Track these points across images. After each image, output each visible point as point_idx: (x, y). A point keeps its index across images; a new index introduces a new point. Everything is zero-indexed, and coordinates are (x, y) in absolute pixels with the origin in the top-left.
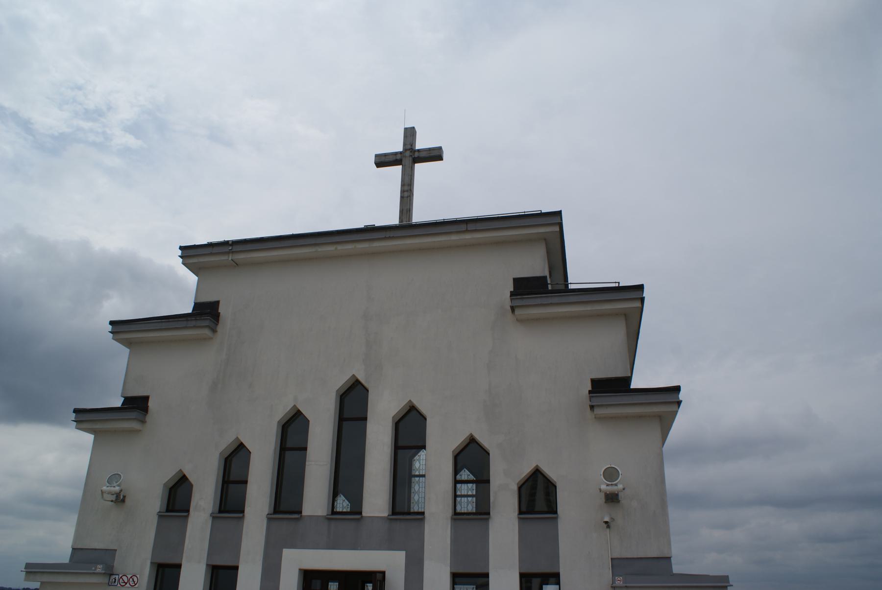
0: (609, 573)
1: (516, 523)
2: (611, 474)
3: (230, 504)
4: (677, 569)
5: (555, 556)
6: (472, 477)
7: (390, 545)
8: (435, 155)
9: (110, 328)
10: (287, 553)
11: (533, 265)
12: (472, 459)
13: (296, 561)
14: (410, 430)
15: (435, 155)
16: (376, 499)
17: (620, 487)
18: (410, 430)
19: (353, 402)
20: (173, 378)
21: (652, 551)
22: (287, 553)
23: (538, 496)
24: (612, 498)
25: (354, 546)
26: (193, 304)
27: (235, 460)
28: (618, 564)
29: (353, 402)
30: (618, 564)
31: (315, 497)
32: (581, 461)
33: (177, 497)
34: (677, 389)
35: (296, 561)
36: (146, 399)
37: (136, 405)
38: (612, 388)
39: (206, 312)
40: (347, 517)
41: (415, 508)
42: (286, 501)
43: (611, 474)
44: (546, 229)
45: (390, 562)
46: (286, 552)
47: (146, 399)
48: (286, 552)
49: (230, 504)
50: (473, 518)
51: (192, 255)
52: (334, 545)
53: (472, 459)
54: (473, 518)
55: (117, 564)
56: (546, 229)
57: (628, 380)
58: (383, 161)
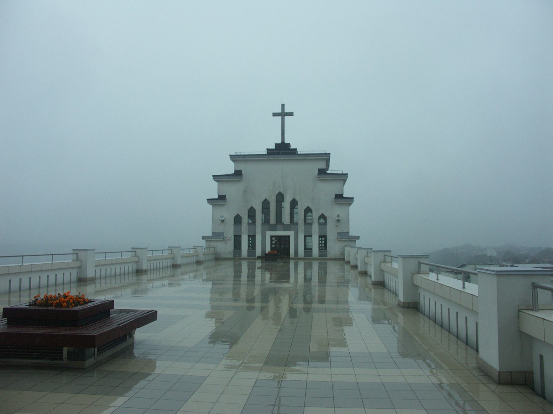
0: (336, 235)
2: (338, 216)
4: (350, 234)
5: (326, 233)
6: (467, 412)
8: (291, 114)
11: (322, 165)
14: (294, 204)
15: (291, 114)
16: (286, 219)
18: (294, 204)
19: (280, 197)
20: (233, 190)
21: (345, 231)
24: (338, 221)
27: (252, 213)
28: (338, 233)
29: (280, 197)
31: (273, 220)
32: (334, 213)
33: (238, 220)
34: (353, 198)
36: (225, 196)
37: (222, 198)
38: (339, 197)
39: (238, 173)
41: (295, 222)
42: (266, 221)
43: (338, 216)
44: (326, 157)
45: (291, 234)
47: (225, 196)
50: (308, 224)
51: (234, 158)
53: (308, 210)
56: (326, 157)
57: (342, 195)
58: (275, 115)
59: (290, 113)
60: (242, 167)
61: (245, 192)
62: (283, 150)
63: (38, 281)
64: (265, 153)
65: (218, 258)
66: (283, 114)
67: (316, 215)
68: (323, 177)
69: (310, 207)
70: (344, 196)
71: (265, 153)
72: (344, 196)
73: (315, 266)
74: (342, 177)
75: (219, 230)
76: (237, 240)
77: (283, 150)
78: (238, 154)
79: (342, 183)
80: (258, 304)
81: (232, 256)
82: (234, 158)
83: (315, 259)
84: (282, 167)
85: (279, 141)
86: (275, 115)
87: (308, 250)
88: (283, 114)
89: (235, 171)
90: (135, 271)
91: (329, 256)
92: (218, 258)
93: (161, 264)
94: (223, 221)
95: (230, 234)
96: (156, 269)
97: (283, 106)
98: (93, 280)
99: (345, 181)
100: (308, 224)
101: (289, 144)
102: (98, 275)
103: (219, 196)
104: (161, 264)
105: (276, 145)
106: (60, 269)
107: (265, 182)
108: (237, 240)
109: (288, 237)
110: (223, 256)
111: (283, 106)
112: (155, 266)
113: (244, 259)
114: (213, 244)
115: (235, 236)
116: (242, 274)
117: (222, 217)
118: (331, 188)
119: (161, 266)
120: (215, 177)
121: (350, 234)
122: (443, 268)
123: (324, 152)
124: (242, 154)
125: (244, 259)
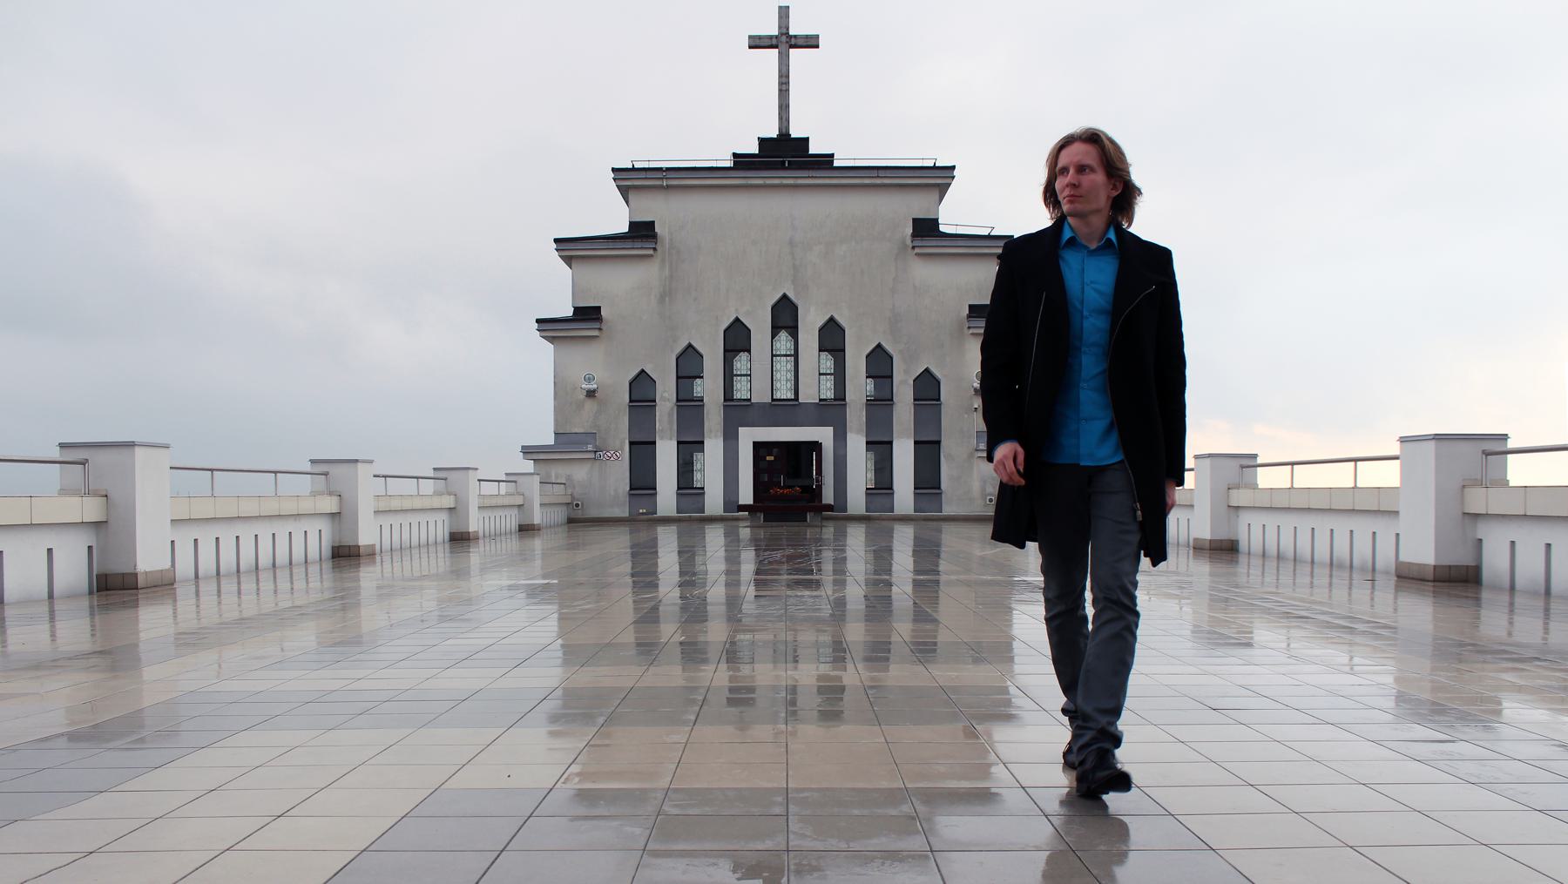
8: (811, 42)
11: (917, 205)
13: (748, 436)
15: (811, 42)
19: (785, 316)
20: (618, 286)
29: (785, 316)
33: (641, 390)
37: (587, 315)
39: (642, 231)
45: (823, 435)
51: (630, 180)
58: (757, 43)
59: (780, 17)
61: (666, 295)
62: (783, 156)
65: (578, 520)
66: (784, 42)
67: (810, 324)
68: (931, 245)
71: (729, 164)
73: (903, 542)
77: (783, 156)
80: (902, 629)
81: (624, 512)
83: (904, 519)
85: (773, 133)
86: (757, 43)
87: (882, 484)
88: (784, 42)
89: (631, 224)
90: (327, 552)
91: (948, 509)
92: (578, 520)
94: (591, 394)
96: (402, 550)
97: (784, 13)
98: (164, 585)
99: (943, 189)
100: (881, 403)
101: (805, 141)
102: (184, 568)
103: (577, 310)
110: (594, 513)
111: (784, 13)
113: (666, 521)
114: (559, 472)
116: (627, 567)
117: (589, 379)
119: (415, 542)
122: (686, 469)
123: (985, 232)
124: (653, 165)
125: (666, 521)
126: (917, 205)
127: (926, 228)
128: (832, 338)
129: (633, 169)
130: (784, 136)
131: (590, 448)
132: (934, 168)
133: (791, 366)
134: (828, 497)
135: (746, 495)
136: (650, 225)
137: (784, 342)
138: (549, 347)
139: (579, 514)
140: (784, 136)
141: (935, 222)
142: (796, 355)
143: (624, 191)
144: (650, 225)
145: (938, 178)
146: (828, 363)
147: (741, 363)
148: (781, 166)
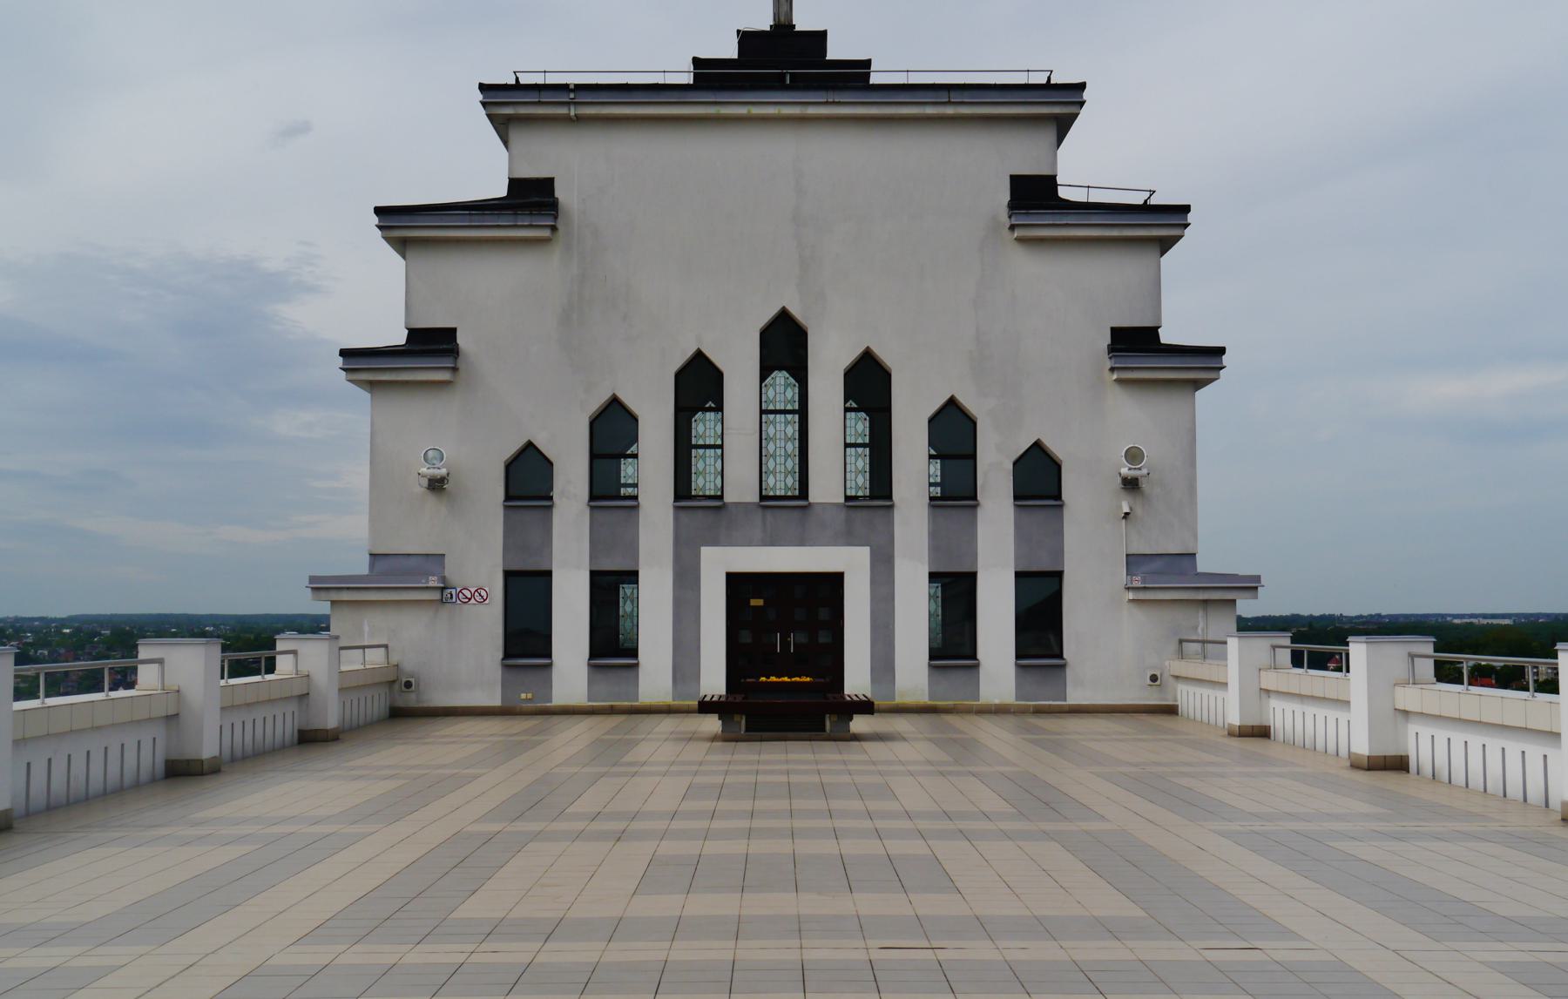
1: (1012, 509)
2: (1134, 456)
3: (608, 491)
4: (1203, 566)
5: (1059, 552)
7: (849, 538)
9: (375, 220)
10: (707, 553)
12: (953, 432)
13: (719, 563)
17: (1145, 471)
19: (784, 345)
20: (486, 293)
22: (707, 553)
23: (1039, 478)
24: (1131, 484)
25: (802, 542)
26: (507, 182)
27: (612, 430)
28: (1134, 561)
29: (784, 345)
30: (1134, 561)
32: (1100, 430)
33: (527, 478)
35: (719, 563)
37: (432, 343)
38: (1135, 343)
39: (531, 198)
40: (788, 507)
45: (850, 561)
46: (866, 550)
48: (866, 550)
49: (608, 491)
50: (956, 493)
51: (510, 105)
52: (772, 541)
53: (953, 432)
54: (956, 493)
55: (451, 571)
57: (1153, 332)
60: (547, 155)
62: (782, 65)
63: (24, 785)
64: (688, 79)
68: (1044, 226)
69: (796, 311)
70: (1166, 337)
71: (688, 79)
72: (1166, 337)
74: (1156, 224)
75: (412, 540)
76: (527, 595)
77: (782, 65)
78: (524, 80)
79: (1050, 134)
82: (510, 105)
84: (781, 157)
91: (1075, 697)
93: (98, 760)
94: (436, 485)
95: (481, 564)
99: (1063, 125)
103: (414, 334)
104: (98, 760)
105: (745, 38)
106: (113, 725)
107: (701, 246)
108: (527, 595)
109: (833, 583)
112: (114, 769)
115: (508, 574)
118: (1097, 288)
120: (379, 211)
121: (1203, 566)
126: (1022, 153)
127: (1034, 195)
128: (868, 384)
129: (518, 87)
130: (783, 28)
131: (433, 582)
132: (1048, 86)
133: (793, 430)
134: (857, 680)
135: (714, 681)
136: (546, 185)
137: (782, 387)
138: (364, 396)
139: (411, 700)
140: (783, 28)
141: (1050, 182)
142: (803, 412)
143: (503, 126)
144: (546, 185)
145: (1056, 106)
146: (860, 426)
147: (704, 427)
148: (774, 84)
